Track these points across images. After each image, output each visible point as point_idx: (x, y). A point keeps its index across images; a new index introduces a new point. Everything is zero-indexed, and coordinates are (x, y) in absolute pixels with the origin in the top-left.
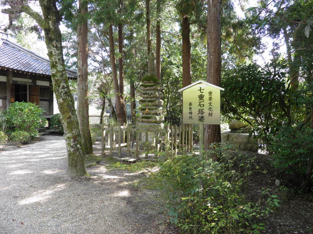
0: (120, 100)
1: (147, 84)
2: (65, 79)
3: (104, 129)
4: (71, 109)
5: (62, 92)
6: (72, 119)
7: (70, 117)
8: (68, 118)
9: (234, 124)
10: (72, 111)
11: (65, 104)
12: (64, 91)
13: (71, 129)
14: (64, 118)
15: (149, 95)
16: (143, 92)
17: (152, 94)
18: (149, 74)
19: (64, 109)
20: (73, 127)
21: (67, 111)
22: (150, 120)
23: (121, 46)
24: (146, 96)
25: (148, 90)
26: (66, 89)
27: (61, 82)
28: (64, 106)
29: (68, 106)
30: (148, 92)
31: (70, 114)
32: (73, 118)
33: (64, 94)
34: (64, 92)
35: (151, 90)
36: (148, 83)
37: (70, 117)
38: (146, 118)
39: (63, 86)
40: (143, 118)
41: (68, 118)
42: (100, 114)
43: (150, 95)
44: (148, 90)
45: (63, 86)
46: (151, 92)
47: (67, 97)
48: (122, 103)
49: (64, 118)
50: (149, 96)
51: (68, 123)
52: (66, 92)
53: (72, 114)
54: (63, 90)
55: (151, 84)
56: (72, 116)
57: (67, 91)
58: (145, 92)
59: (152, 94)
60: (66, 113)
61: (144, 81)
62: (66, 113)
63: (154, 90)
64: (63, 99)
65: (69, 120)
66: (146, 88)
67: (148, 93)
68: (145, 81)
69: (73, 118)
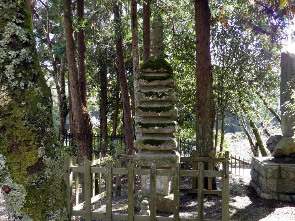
0: (82, 108)
1: (151, 75)
2: (21, 11)
3: (71, 170)
4: (43, 131)
5: (9, 62)
6: (47, 172)
7: (39, 166)
8: (31, 170)
9: (285, 148)
10: (46, 142)
11: (20, 113)
12: (18, 56)
13: (44, 211)
14: (15, 168)
15: (158, 97)
16: (145, 91)
17: (163, 94)
18: (154, 57)
19: (15, 133)
20: (51, 201)
21: (26, 142)
22: (162, 147)
23: (81, 14)
24: (151, 98)
25: (155, 87)
26: (23, 50)
27: (7, 20)
28: (15, 120)
29: (31, 120)
30: (155, 91)
31: (41, 151)
32: (52, 168)
33: (17, 68)
34: (17, 61)
35: (161, 86)
36: (154, 73)
37: (39, 166)
38: (152, 142)
39: (14, 36)
40: (146, 142)
41: (31, 170)
42: (240, 160)
43: (161, 97)
44: (155, 87)
45: (14, 36)
46: (161, 91)
47: (30, 84)
48: (84, 113)
49: (15, 168)
50: (159, 99)
51: (30, 189)
52: (25, 65)
53: (49, 152)
54: (13, 53)
55: (161, 75)
56: (47, 161)
57: (30, 59)
58: (148, 91)
59: (163, 94)
60: (23, 148)
61: (146, 68)
62: (23, 148)
63: (167, 86)
64: (13, 92)
65: (34, 178)
66: (152, 83)
67: (157, 93)
68: (148, 70)
69: (52, 168)
